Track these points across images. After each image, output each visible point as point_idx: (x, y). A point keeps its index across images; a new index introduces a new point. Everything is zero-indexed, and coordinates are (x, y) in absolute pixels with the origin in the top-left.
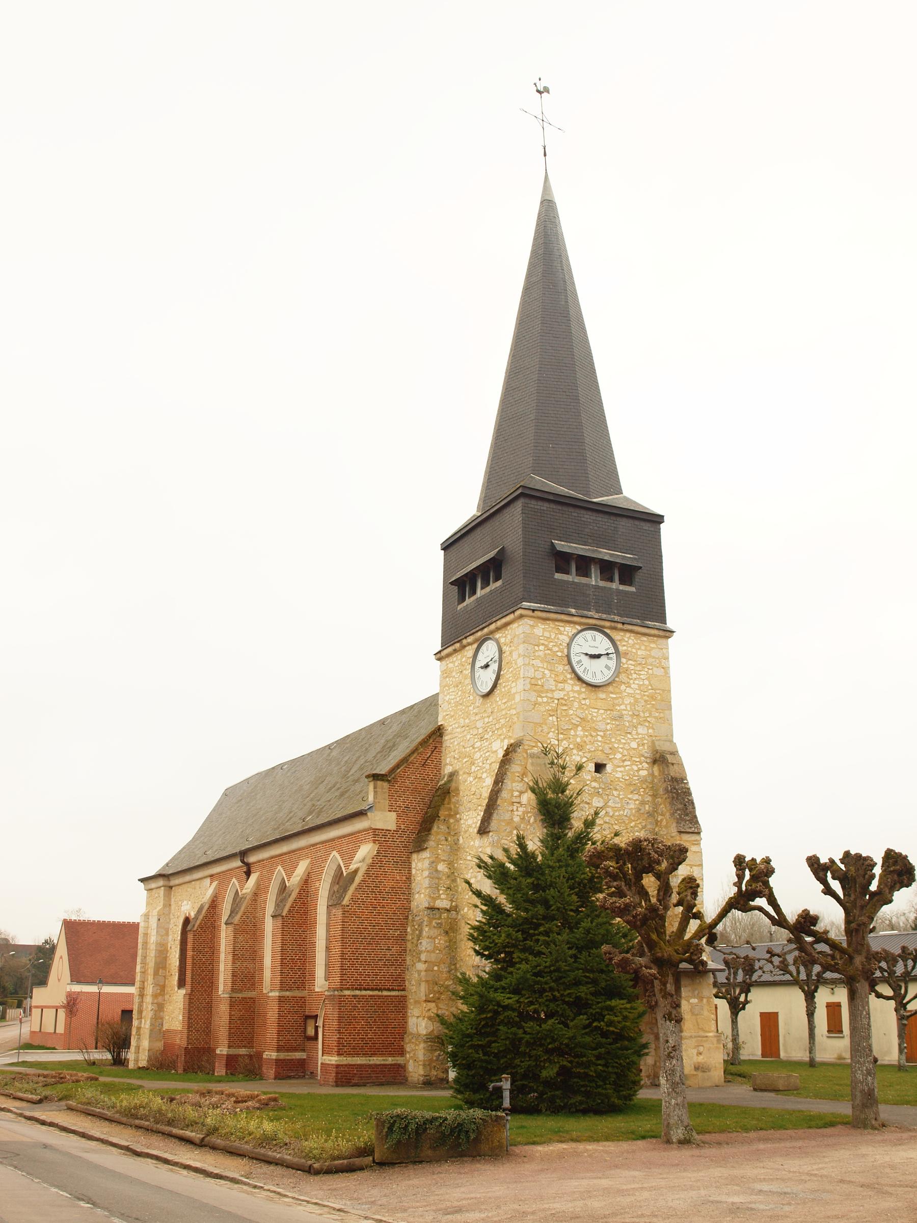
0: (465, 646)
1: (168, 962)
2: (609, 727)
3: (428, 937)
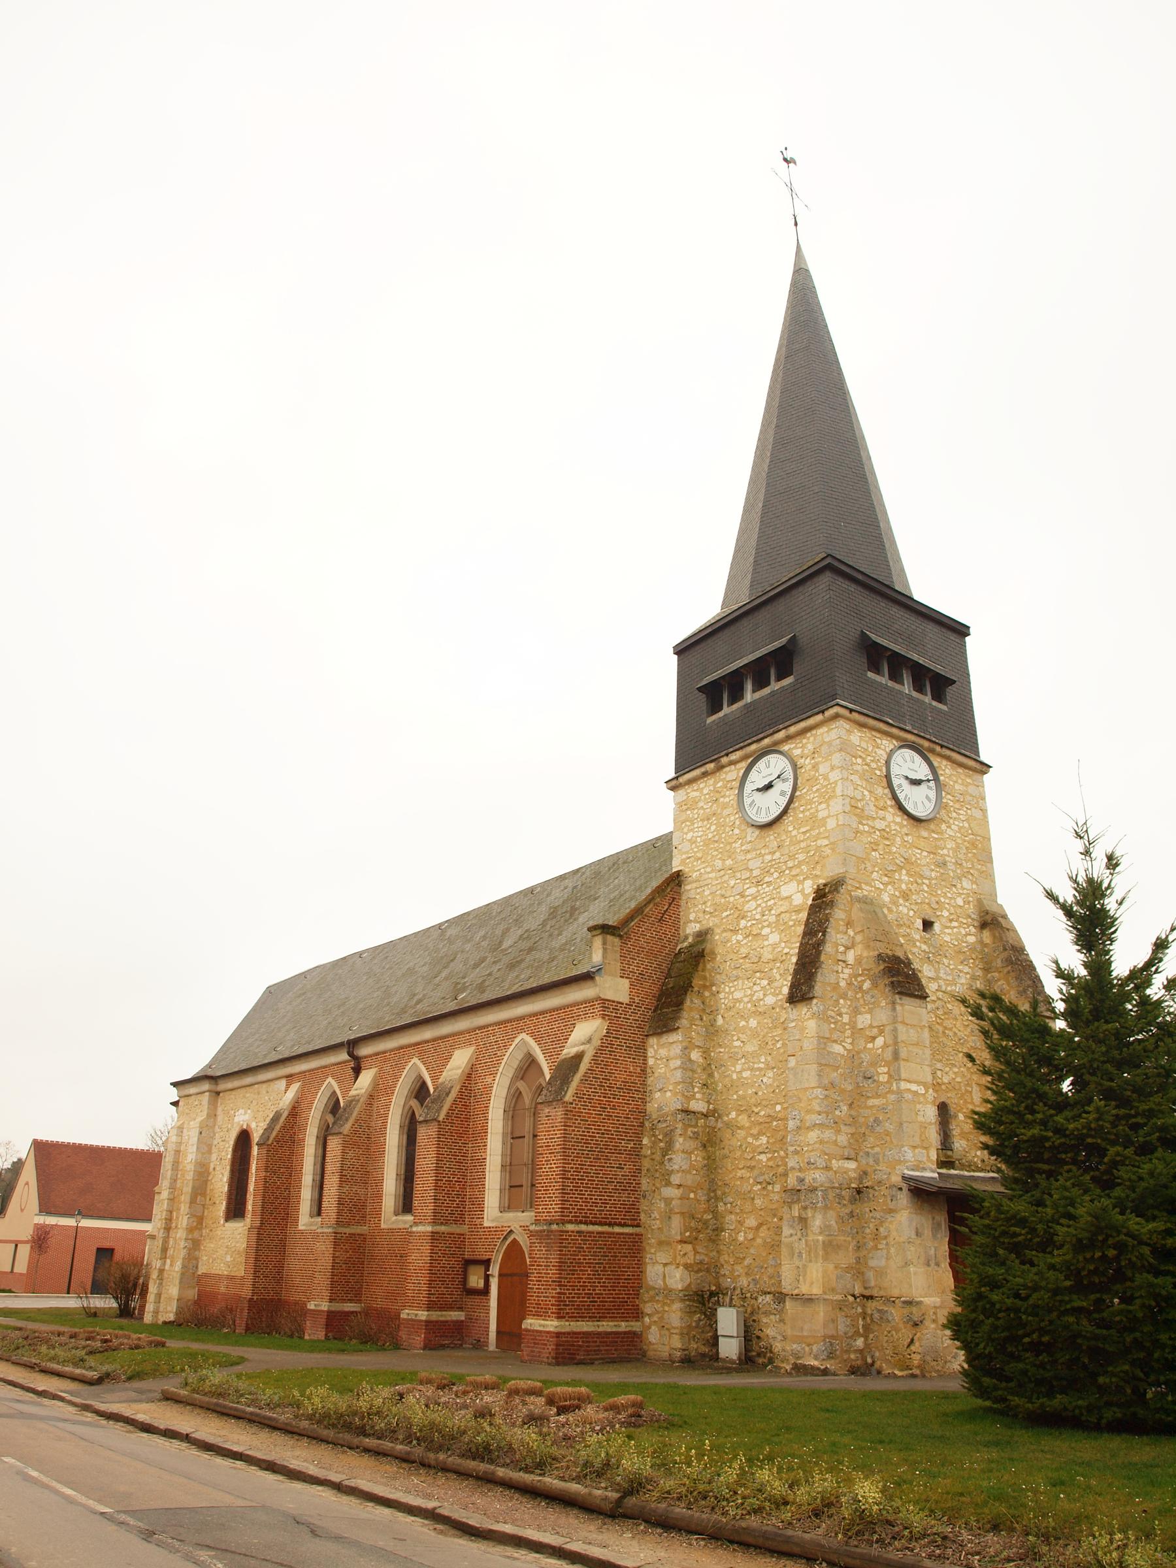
0: (723, 767)
1: (209, 1187)
3: (683, 1151)
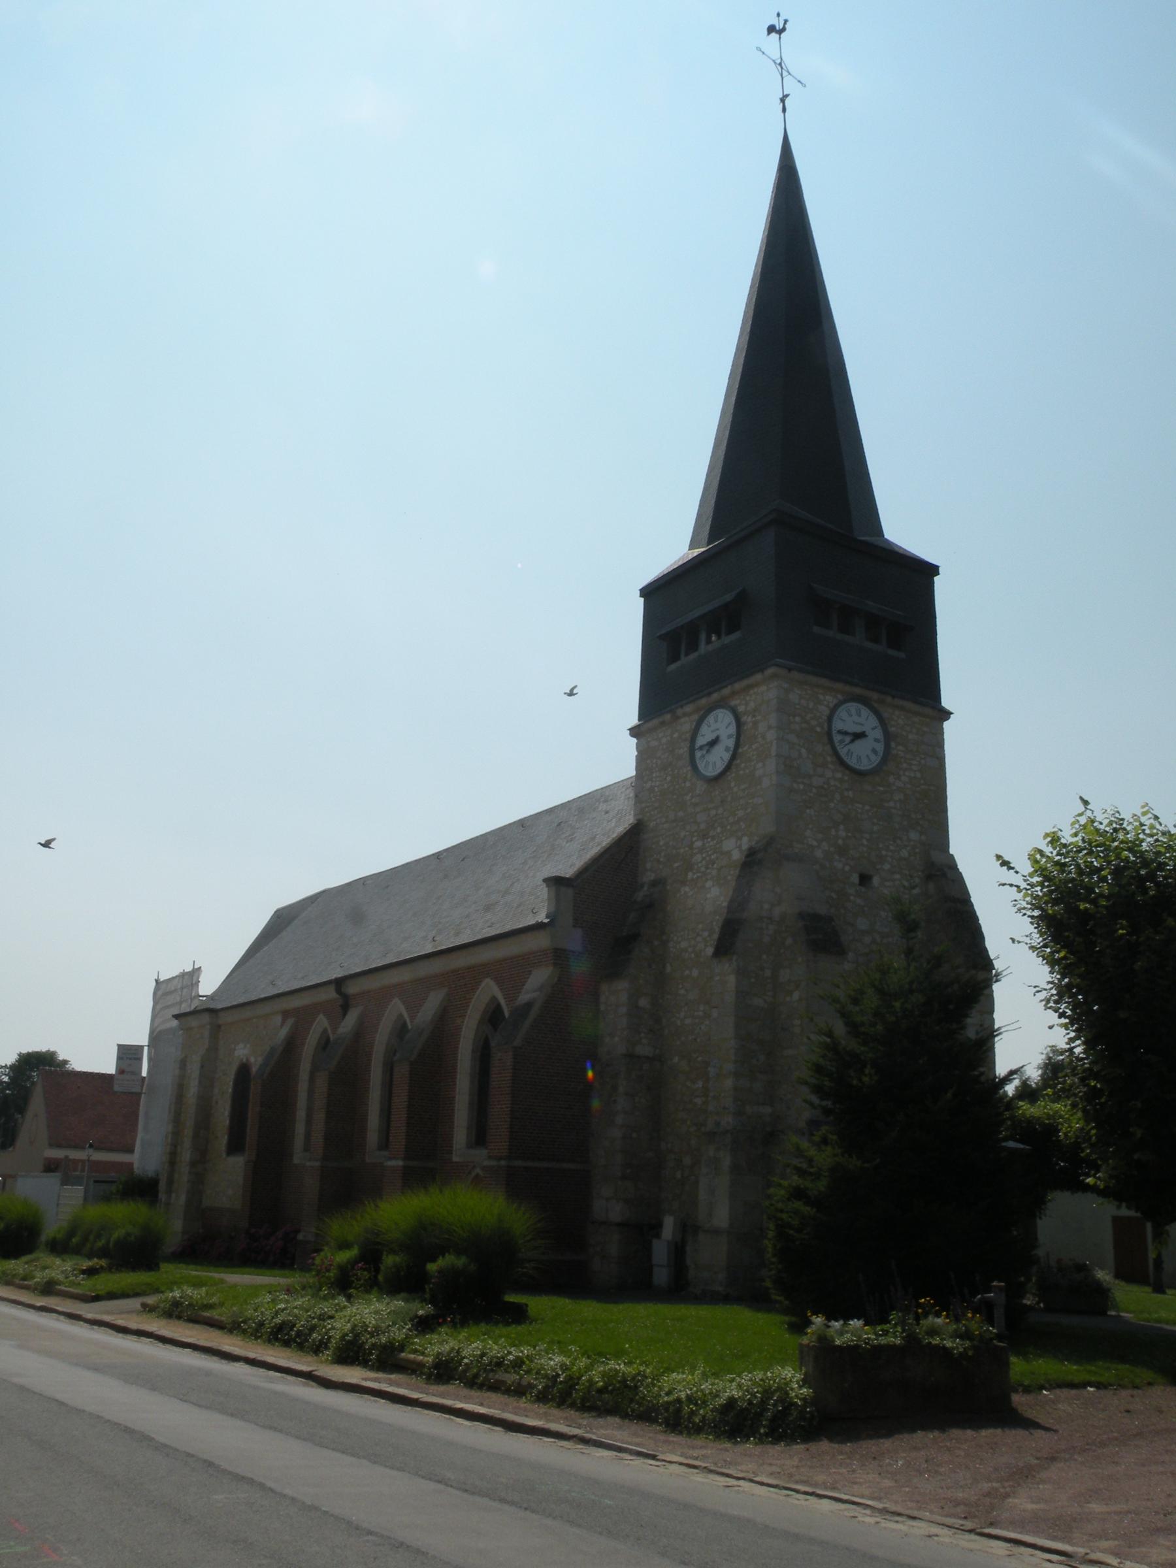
0: (678, 718)
2: (875, 828)
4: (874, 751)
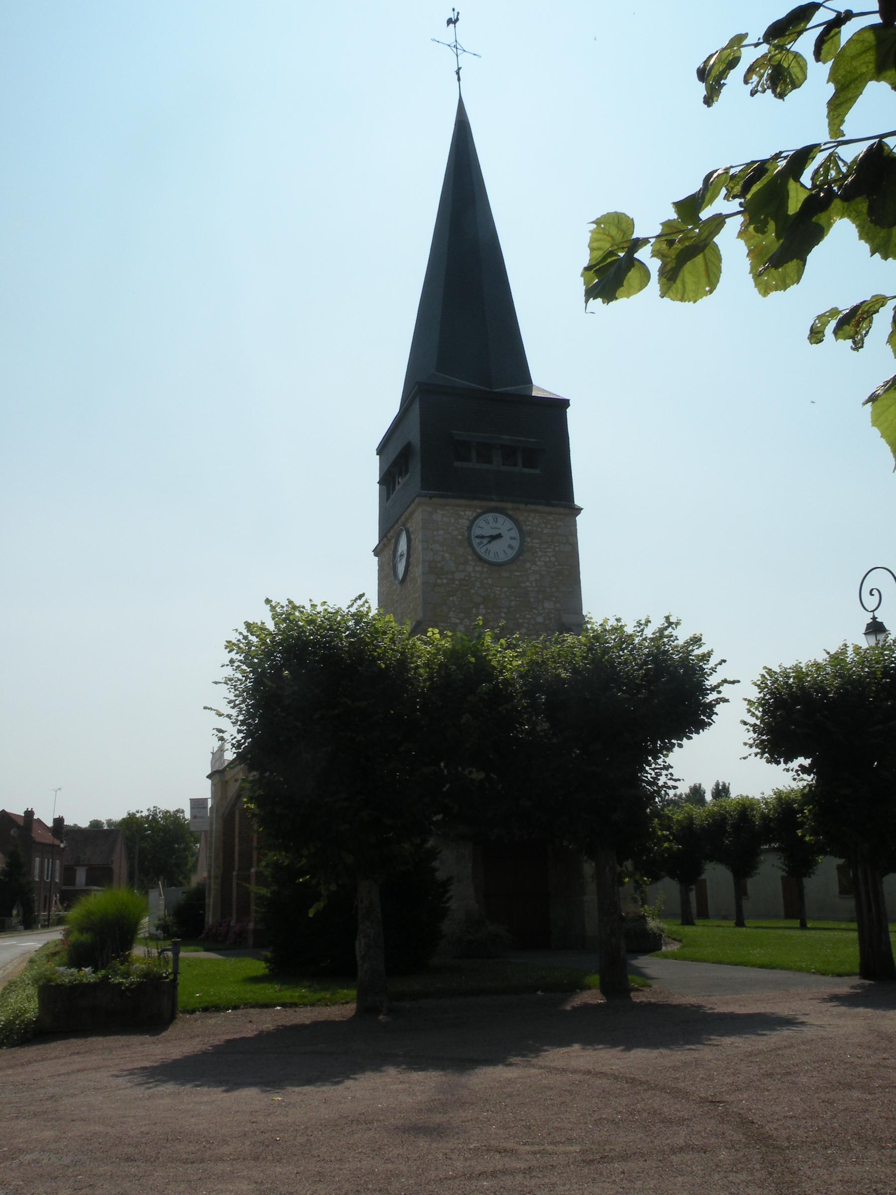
4: (511, 547)
